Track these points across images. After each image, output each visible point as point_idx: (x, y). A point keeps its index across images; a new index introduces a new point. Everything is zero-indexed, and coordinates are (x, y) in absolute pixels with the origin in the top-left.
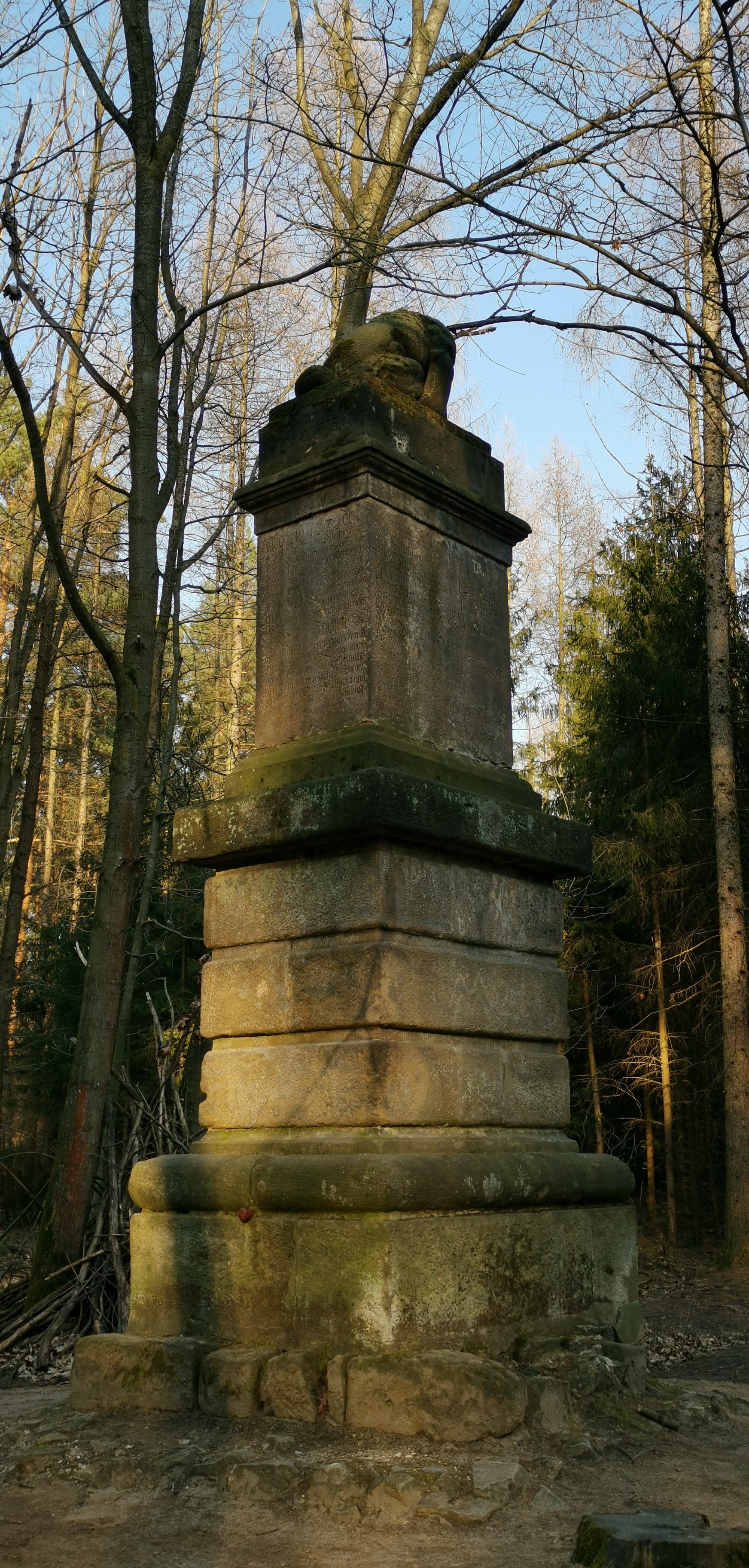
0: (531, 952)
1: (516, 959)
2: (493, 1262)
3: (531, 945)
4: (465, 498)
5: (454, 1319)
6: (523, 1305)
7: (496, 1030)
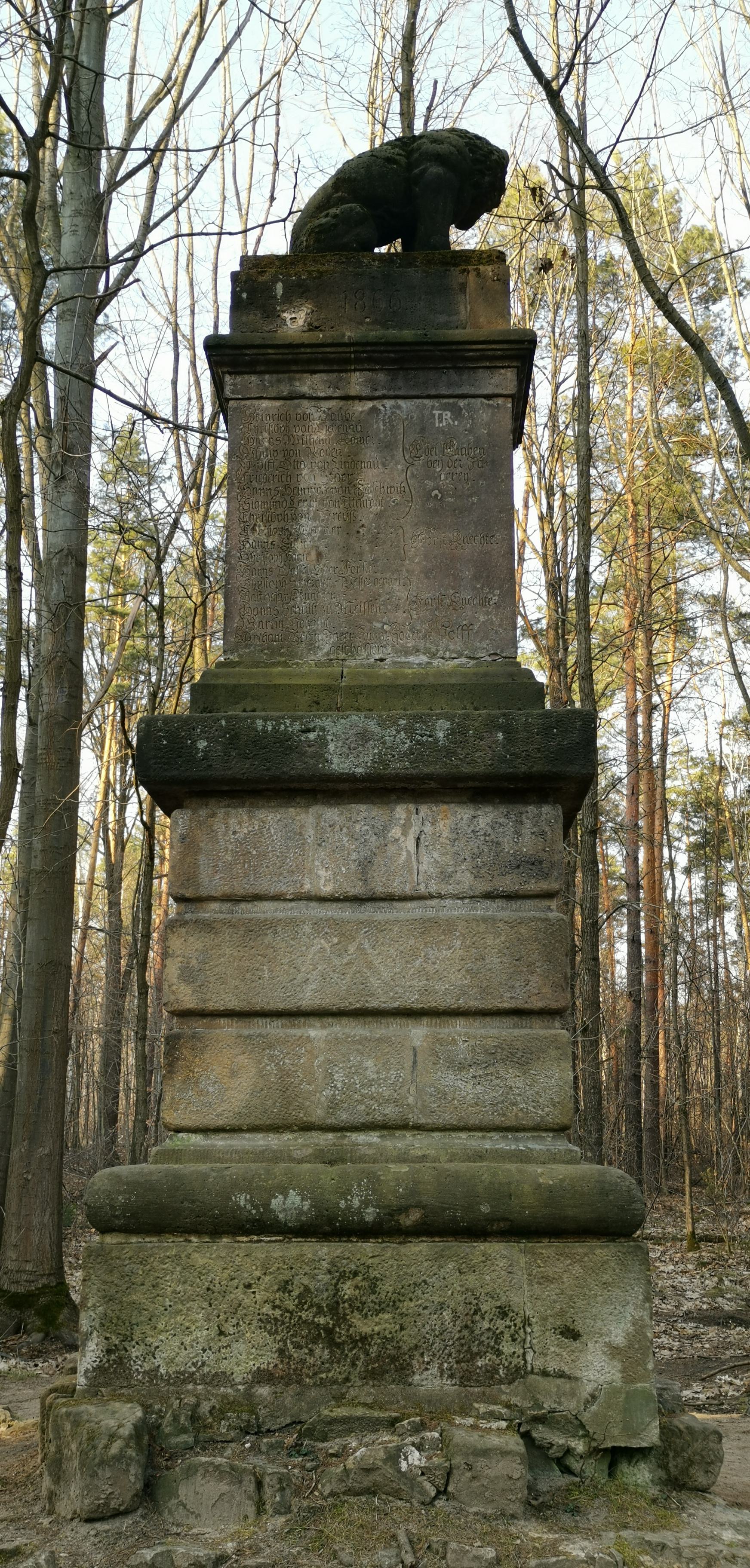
0: (489, 896)
2: (290, 1305)
3: (482, 887)
5: (206, 1369)
6: (353, 1364)
7: (396, 1005)
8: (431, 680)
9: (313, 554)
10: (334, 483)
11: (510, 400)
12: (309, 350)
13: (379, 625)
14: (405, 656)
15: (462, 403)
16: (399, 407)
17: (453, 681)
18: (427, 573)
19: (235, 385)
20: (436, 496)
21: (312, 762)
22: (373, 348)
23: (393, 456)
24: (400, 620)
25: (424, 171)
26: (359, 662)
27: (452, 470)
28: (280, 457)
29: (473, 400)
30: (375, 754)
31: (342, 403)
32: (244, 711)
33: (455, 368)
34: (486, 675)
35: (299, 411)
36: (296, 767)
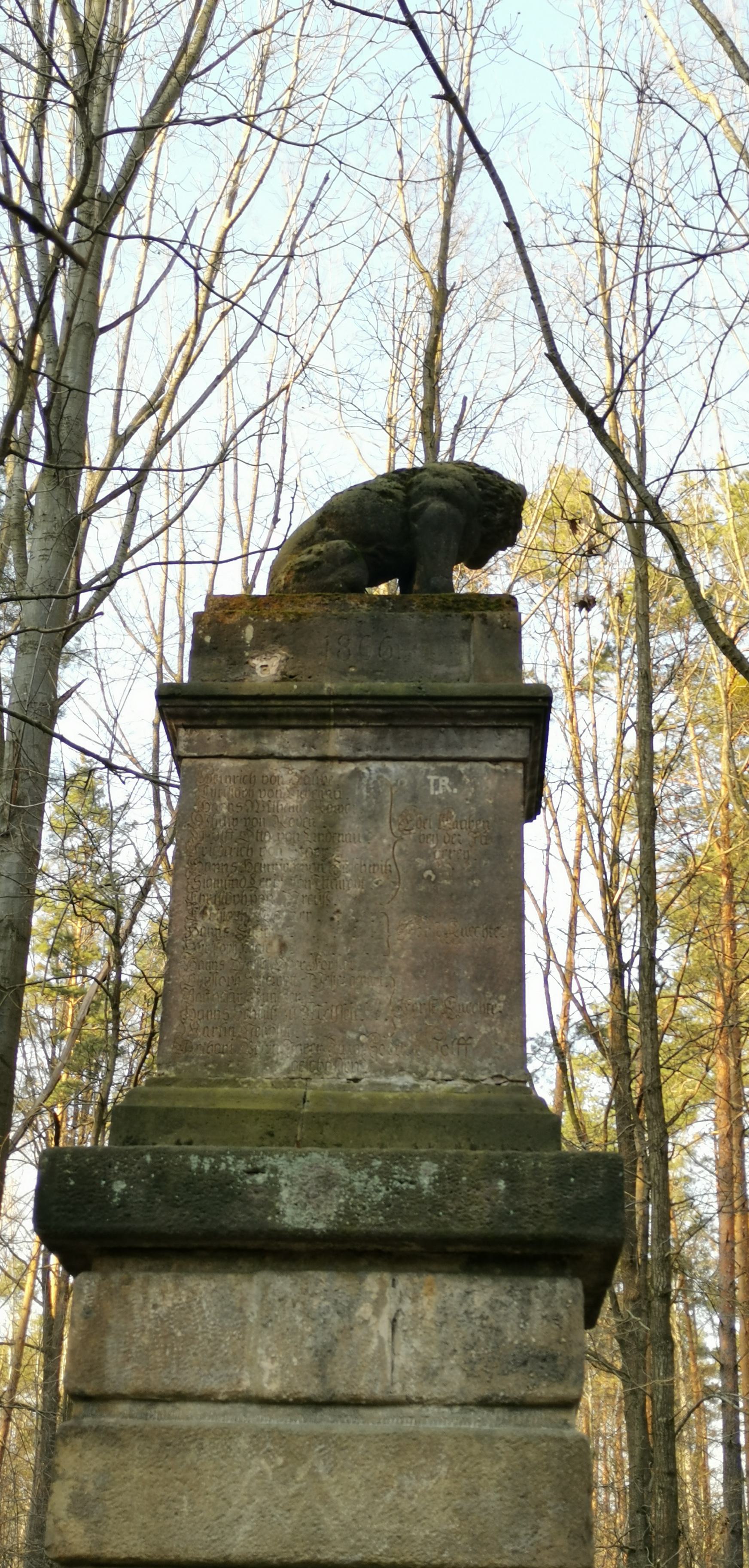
0: (485, 1403)
1: (440, 1422)
3: (477, 1390)
4: (374, 697)
9: (276, 944)
10: (304, 859)
11: (521, 765)
12: (280, 703)
13: (352, 1035)
15: (462, 767)
16: (386, 771)
17: (445, 1110)
18: (416, 971)
20: (429, 877)
21: (258, 1213)
23: (377, 829)
24: (381, 1030)
25: (425, 506)
30: (340, 1205)
33: (454, 726)
35: (266, 773)
36: (237, 1219)
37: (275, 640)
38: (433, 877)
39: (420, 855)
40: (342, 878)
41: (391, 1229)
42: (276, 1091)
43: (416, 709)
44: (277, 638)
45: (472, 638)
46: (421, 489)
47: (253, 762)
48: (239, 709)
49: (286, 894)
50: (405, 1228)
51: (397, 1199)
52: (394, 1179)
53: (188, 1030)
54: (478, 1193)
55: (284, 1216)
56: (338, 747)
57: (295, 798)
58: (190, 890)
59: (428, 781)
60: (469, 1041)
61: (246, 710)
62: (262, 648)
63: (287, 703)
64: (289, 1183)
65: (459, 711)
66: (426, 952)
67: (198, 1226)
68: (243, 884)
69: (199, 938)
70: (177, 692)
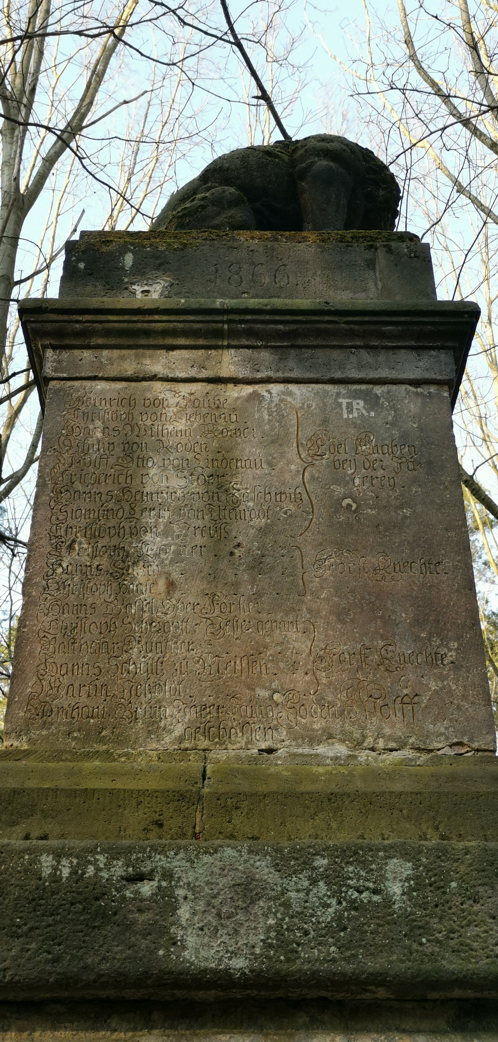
8: (359, 784)
9: (162, 584)
10: (196, 487)
11: (446, 388)
12: (165, 318)
13: (263, 693)
14: (311, 744)
15: (378, 390)
16: (290, 394)
17: (397, 787)
18: (341, 614)
19: (59, 362)
20: (349, 506)
21: (144, 944)
22: (254, 317)
23: (282, 455)
24: (300, 686)
25: (312, 164)
26: (232, 753)
27: (371, 473)
28: (118, 451)
29: (394, 388)
30: (269, 929)
31: (210, 387)
32: (27, 837)
33: (367, 347)
34: (452, 778)
35: (149, 395)
36: (108, 956)
37: (158, 267)
38: (354, 506)
39: (336, 482)
40: (242, 507)
41: (349, 968)
42: (165, 766)
43: (323, 326)
44: (160, 265)
45: (377, 267)
46: (306, 151)
47: (133, 384)
48: (116, 325)
49: (175, 527)
50: (373, 964)
51: (356, 918)
52: (350, 887)
53: (46, 688)
54: (477, 907)
55: (184, 948)
56: (232, 368)
57: (184, 421)
58: (54, 522)
59: (340, 405)
60: (416, 699)
61: (125, 325)
62: (143, 274)
63: (172, 318)
64: (190, 896)
65: (372, 327)
66: (352, 592)
67: (49, 968)
68: (120, 514)
69: (65, 576)
70: (44, 305)
